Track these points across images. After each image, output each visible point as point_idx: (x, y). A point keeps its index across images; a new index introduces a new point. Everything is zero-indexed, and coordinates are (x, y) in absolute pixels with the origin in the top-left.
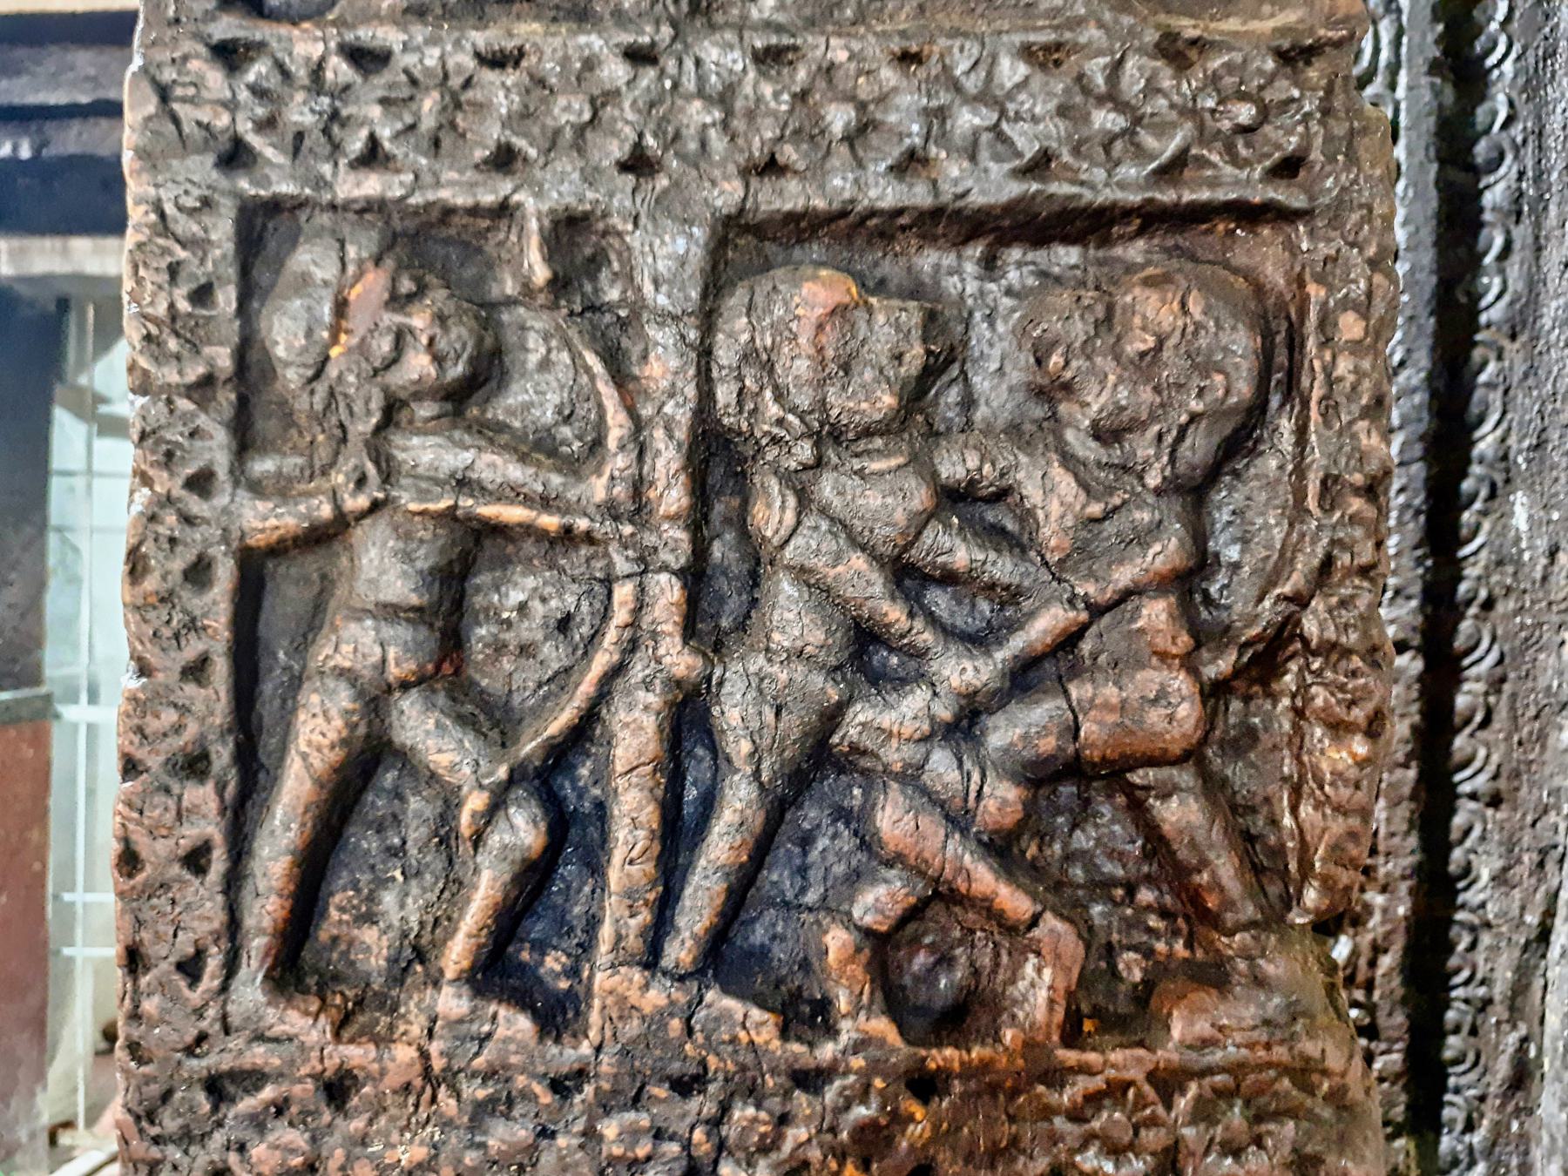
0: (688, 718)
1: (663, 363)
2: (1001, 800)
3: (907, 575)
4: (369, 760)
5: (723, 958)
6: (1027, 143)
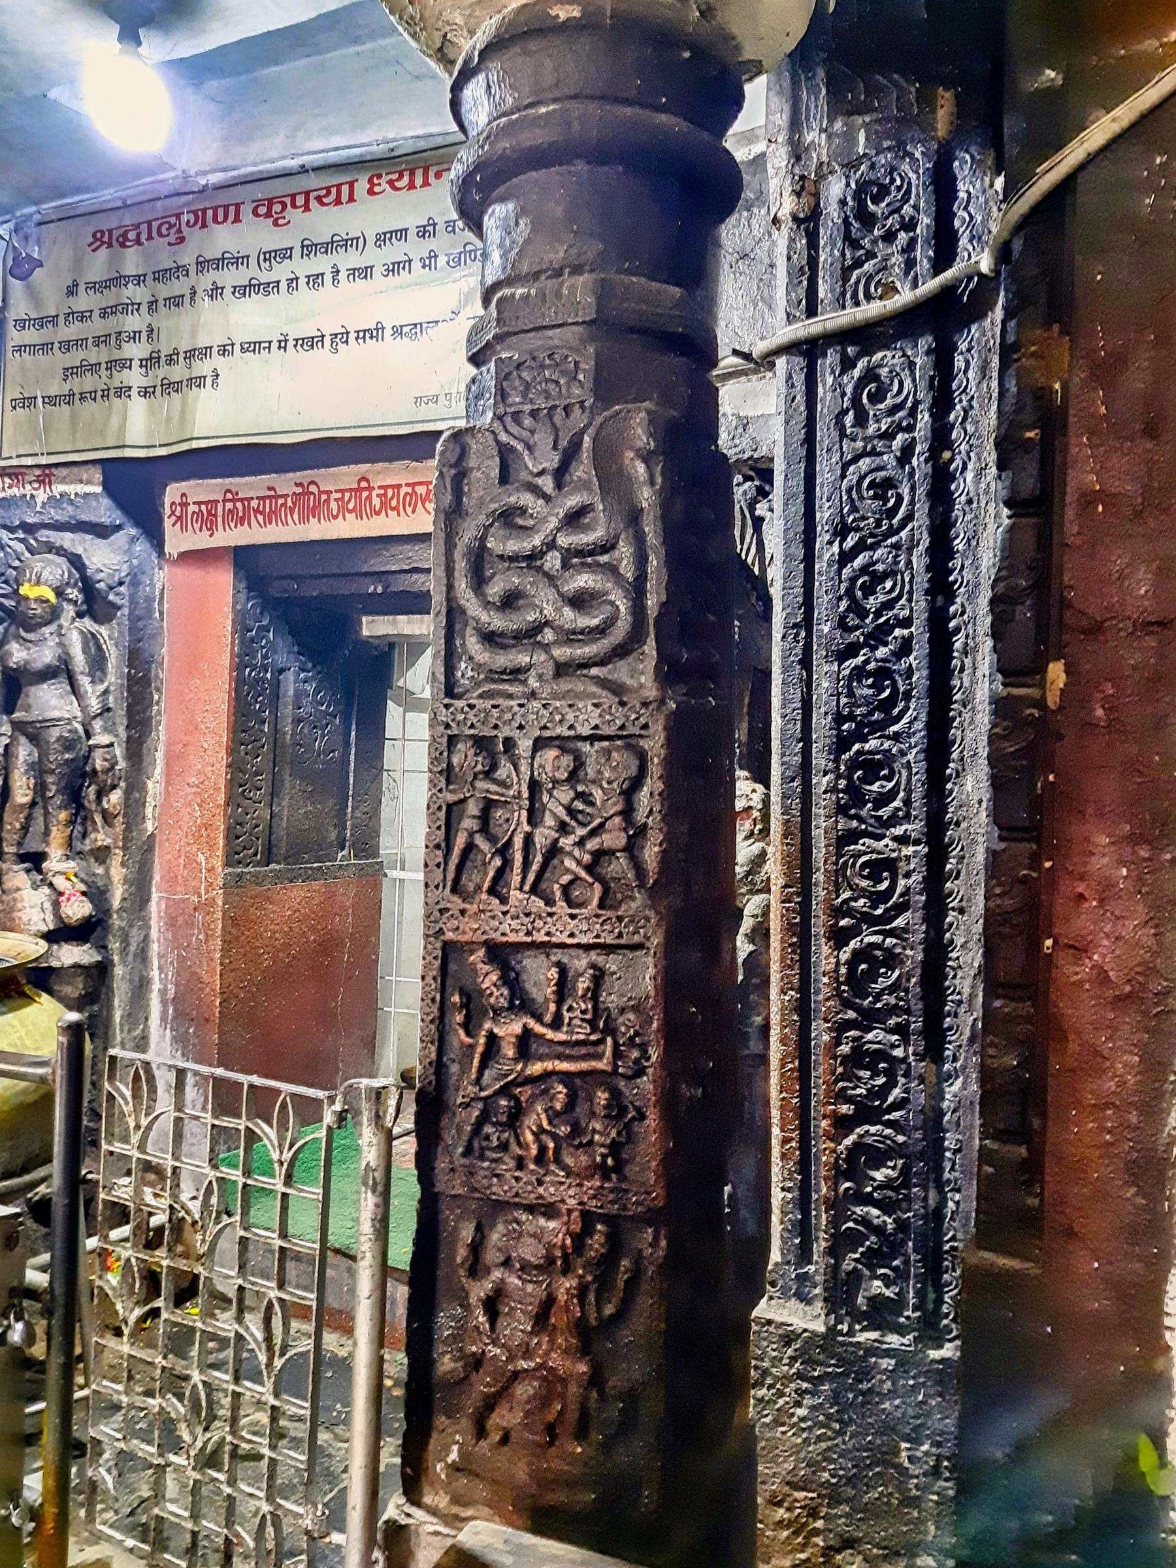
0: (528, 839)
1: (524, 768)
2: (587, 858)
3: (570, 811)
4: (470, 847)
5: (534, 890)
6: (593, 722)
